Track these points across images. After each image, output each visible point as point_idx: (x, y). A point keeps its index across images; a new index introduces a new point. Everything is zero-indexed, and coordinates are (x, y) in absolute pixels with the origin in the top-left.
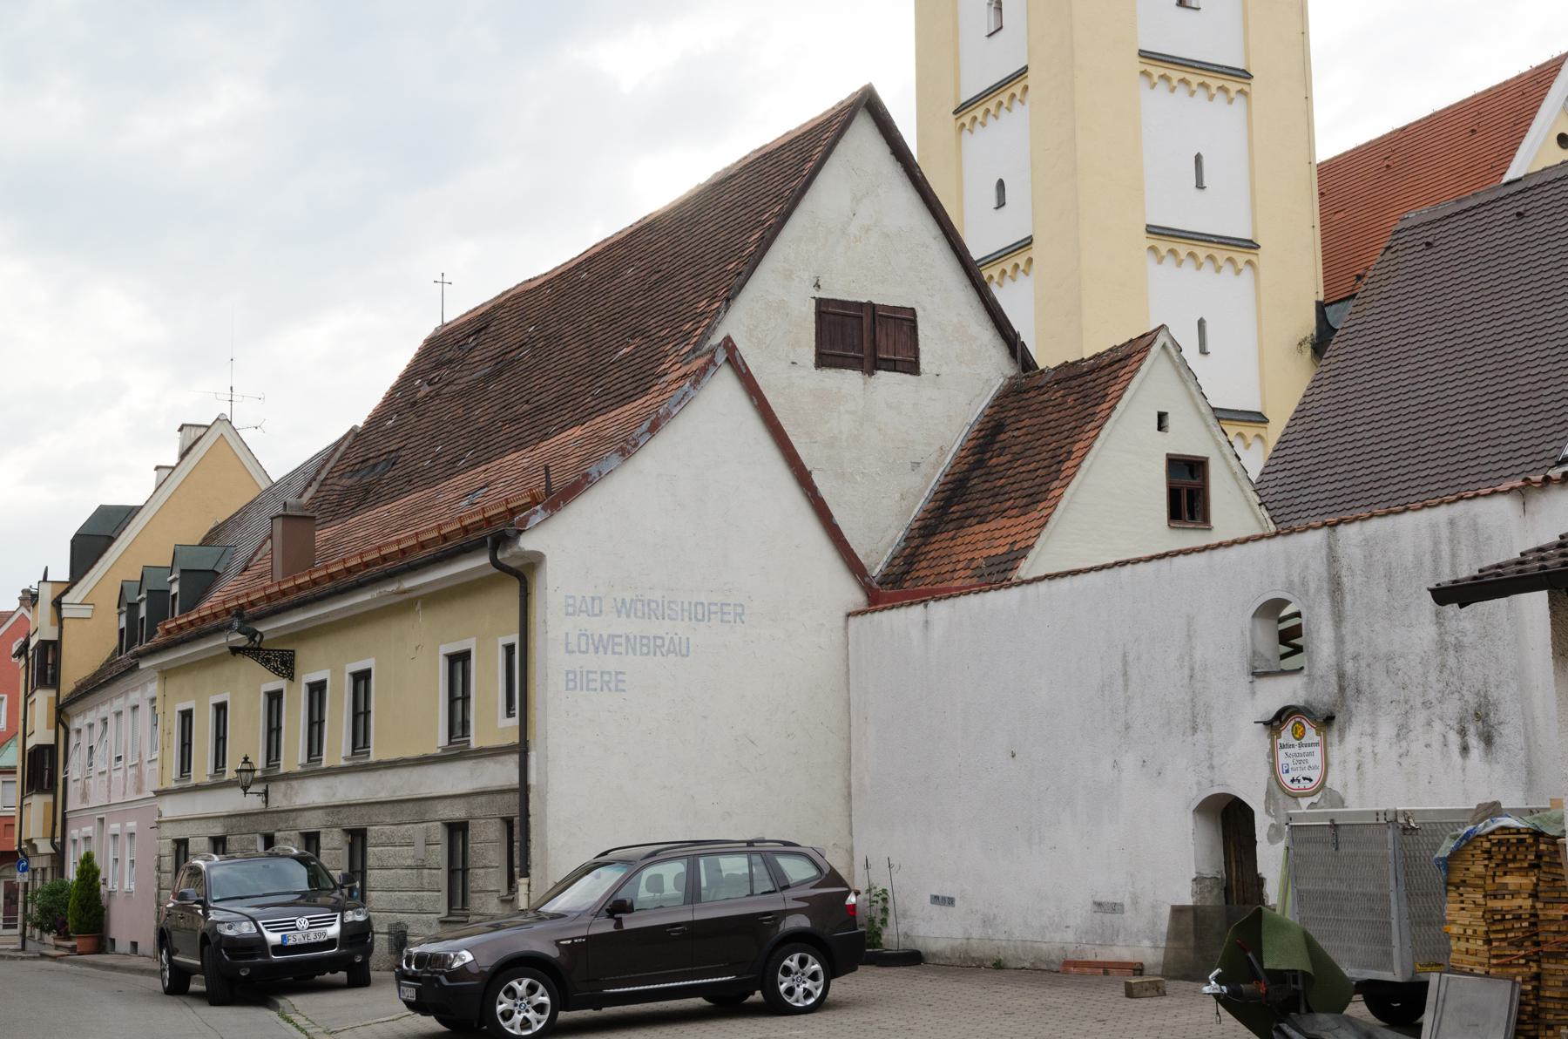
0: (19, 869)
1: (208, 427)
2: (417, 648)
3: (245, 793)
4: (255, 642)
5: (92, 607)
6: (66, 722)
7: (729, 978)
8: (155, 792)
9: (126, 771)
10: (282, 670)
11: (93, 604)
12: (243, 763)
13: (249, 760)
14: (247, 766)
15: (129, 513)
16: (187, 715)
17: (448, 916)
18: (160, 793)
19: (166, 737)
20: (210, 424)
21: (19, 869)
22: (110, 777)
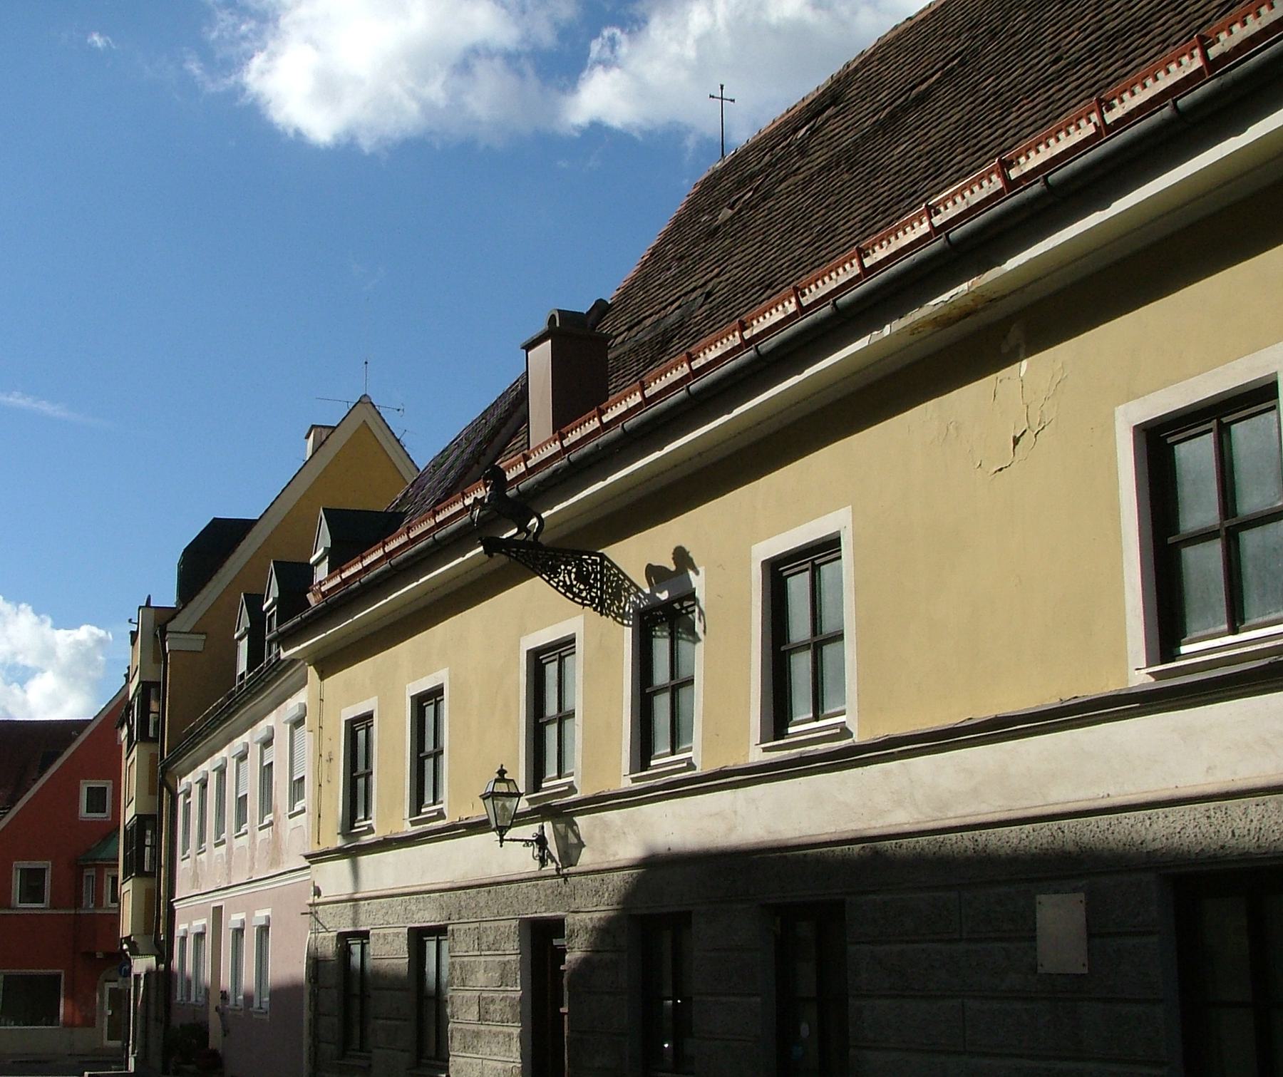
0: (121, 973)
1: (334, 428)
2: (1016, 441)
3: (502, 841)
4: (528, 532)
5: (204, 637)
6: (172, 784)
7: (142, 989)
8: (307, 857)
9: (254, 836)
10: (581, 591)
11: (206, 633)
12: (496, 781)
13: (506, 776)
14: (503, 788)
15: (246, 526)
16: (358, 729)
17: (259, 1008)
18: (314, 858)
19: (325, 764)
20: (335, 425)
21: (121, 973)
22: (229, 850)
